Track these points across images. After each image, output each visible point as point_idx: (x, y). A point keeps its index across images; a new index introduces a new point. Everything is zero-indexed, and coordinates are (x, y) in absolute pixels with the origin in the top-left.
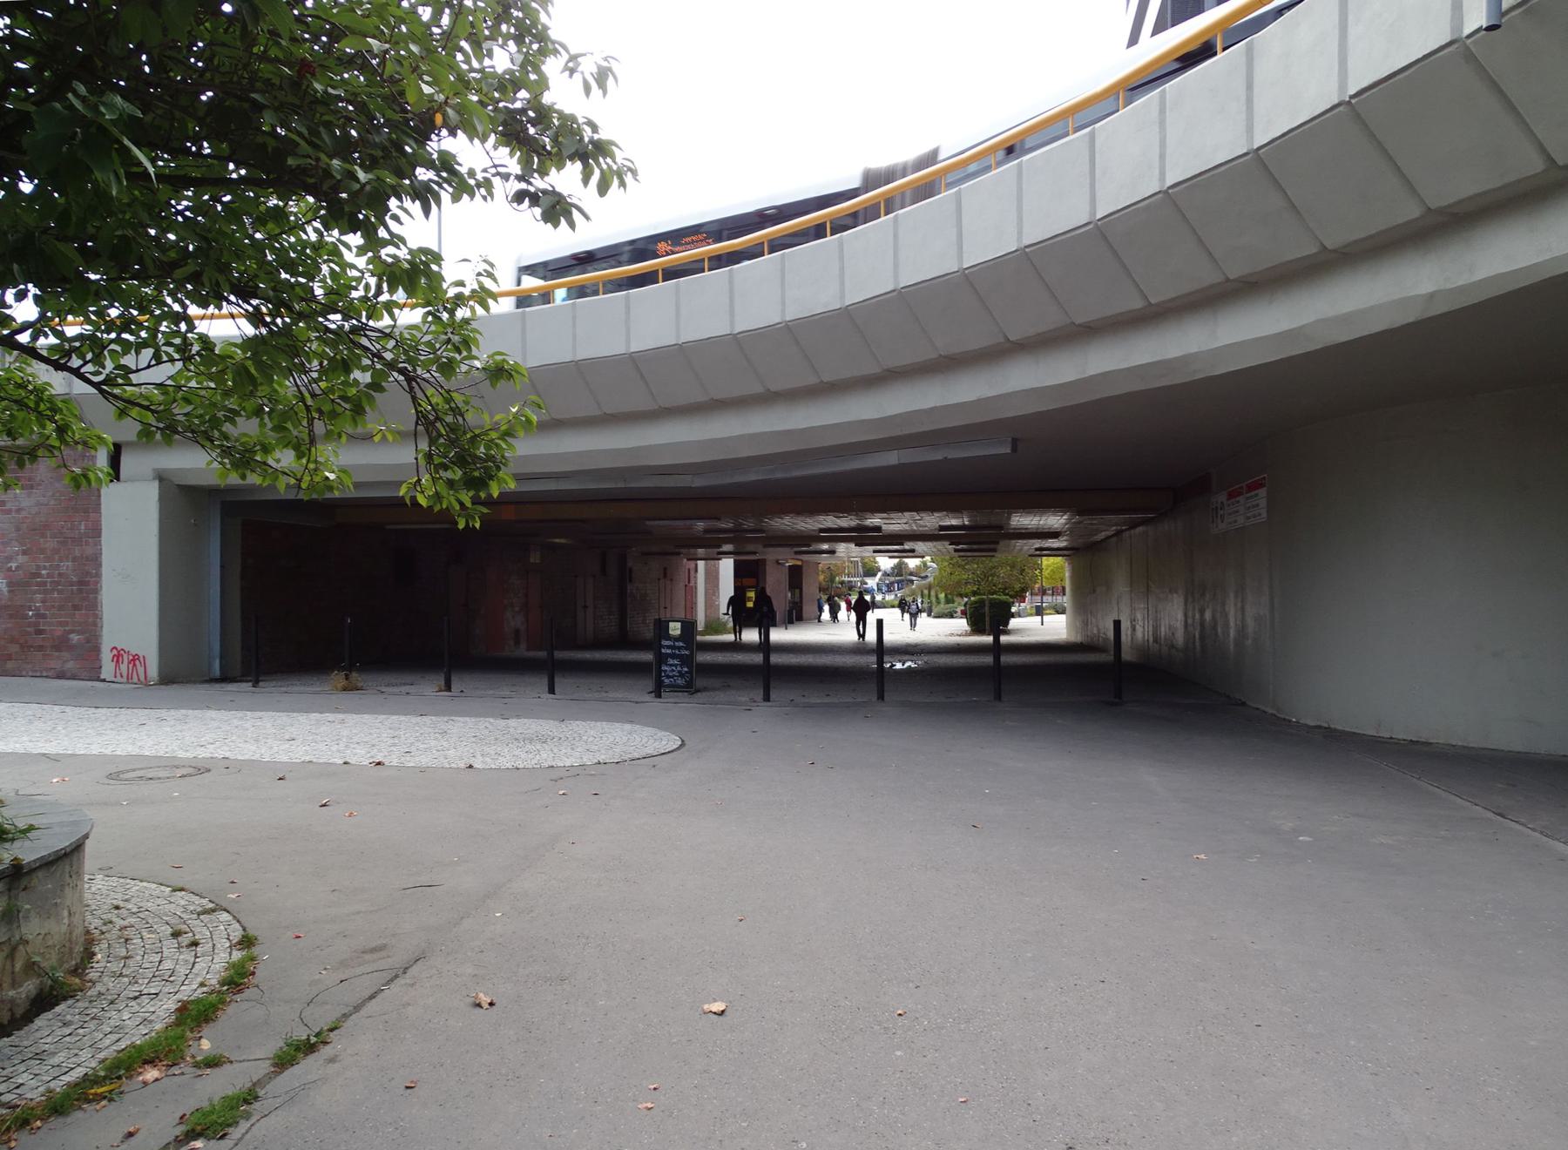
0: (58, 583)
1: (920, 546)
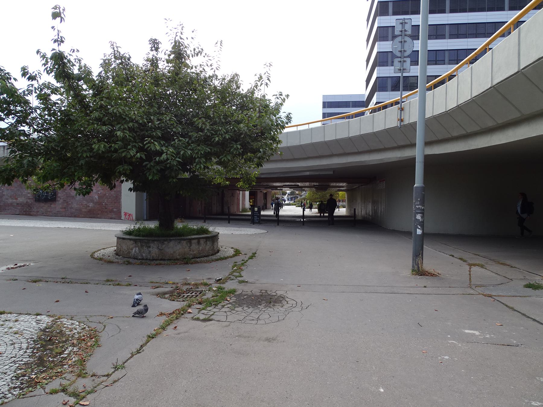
0: (111, 197)
1: (306, 189)
